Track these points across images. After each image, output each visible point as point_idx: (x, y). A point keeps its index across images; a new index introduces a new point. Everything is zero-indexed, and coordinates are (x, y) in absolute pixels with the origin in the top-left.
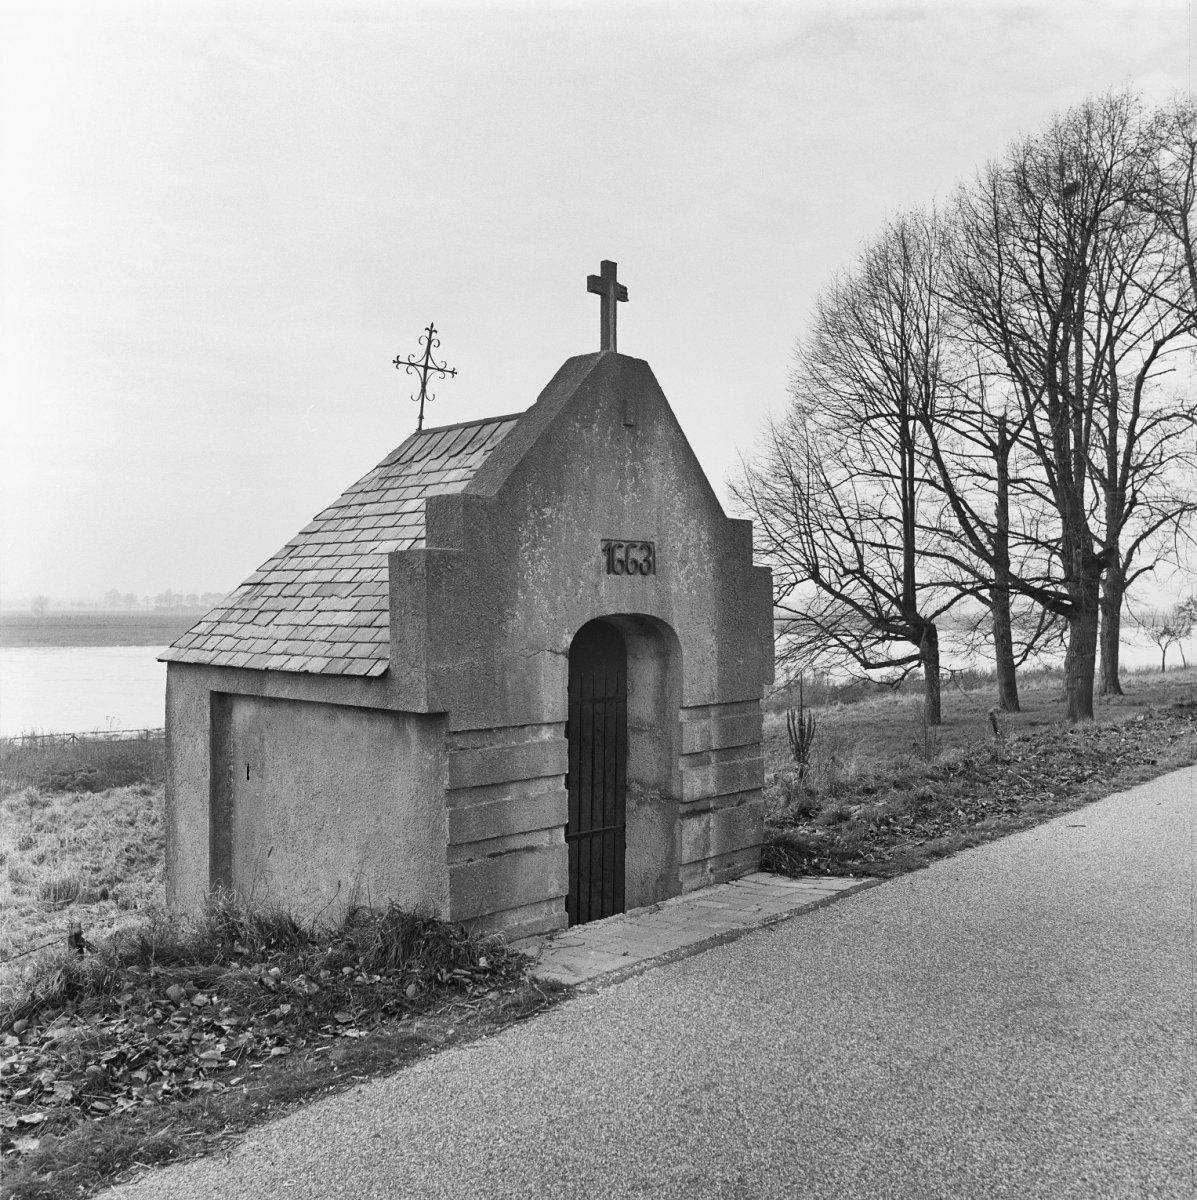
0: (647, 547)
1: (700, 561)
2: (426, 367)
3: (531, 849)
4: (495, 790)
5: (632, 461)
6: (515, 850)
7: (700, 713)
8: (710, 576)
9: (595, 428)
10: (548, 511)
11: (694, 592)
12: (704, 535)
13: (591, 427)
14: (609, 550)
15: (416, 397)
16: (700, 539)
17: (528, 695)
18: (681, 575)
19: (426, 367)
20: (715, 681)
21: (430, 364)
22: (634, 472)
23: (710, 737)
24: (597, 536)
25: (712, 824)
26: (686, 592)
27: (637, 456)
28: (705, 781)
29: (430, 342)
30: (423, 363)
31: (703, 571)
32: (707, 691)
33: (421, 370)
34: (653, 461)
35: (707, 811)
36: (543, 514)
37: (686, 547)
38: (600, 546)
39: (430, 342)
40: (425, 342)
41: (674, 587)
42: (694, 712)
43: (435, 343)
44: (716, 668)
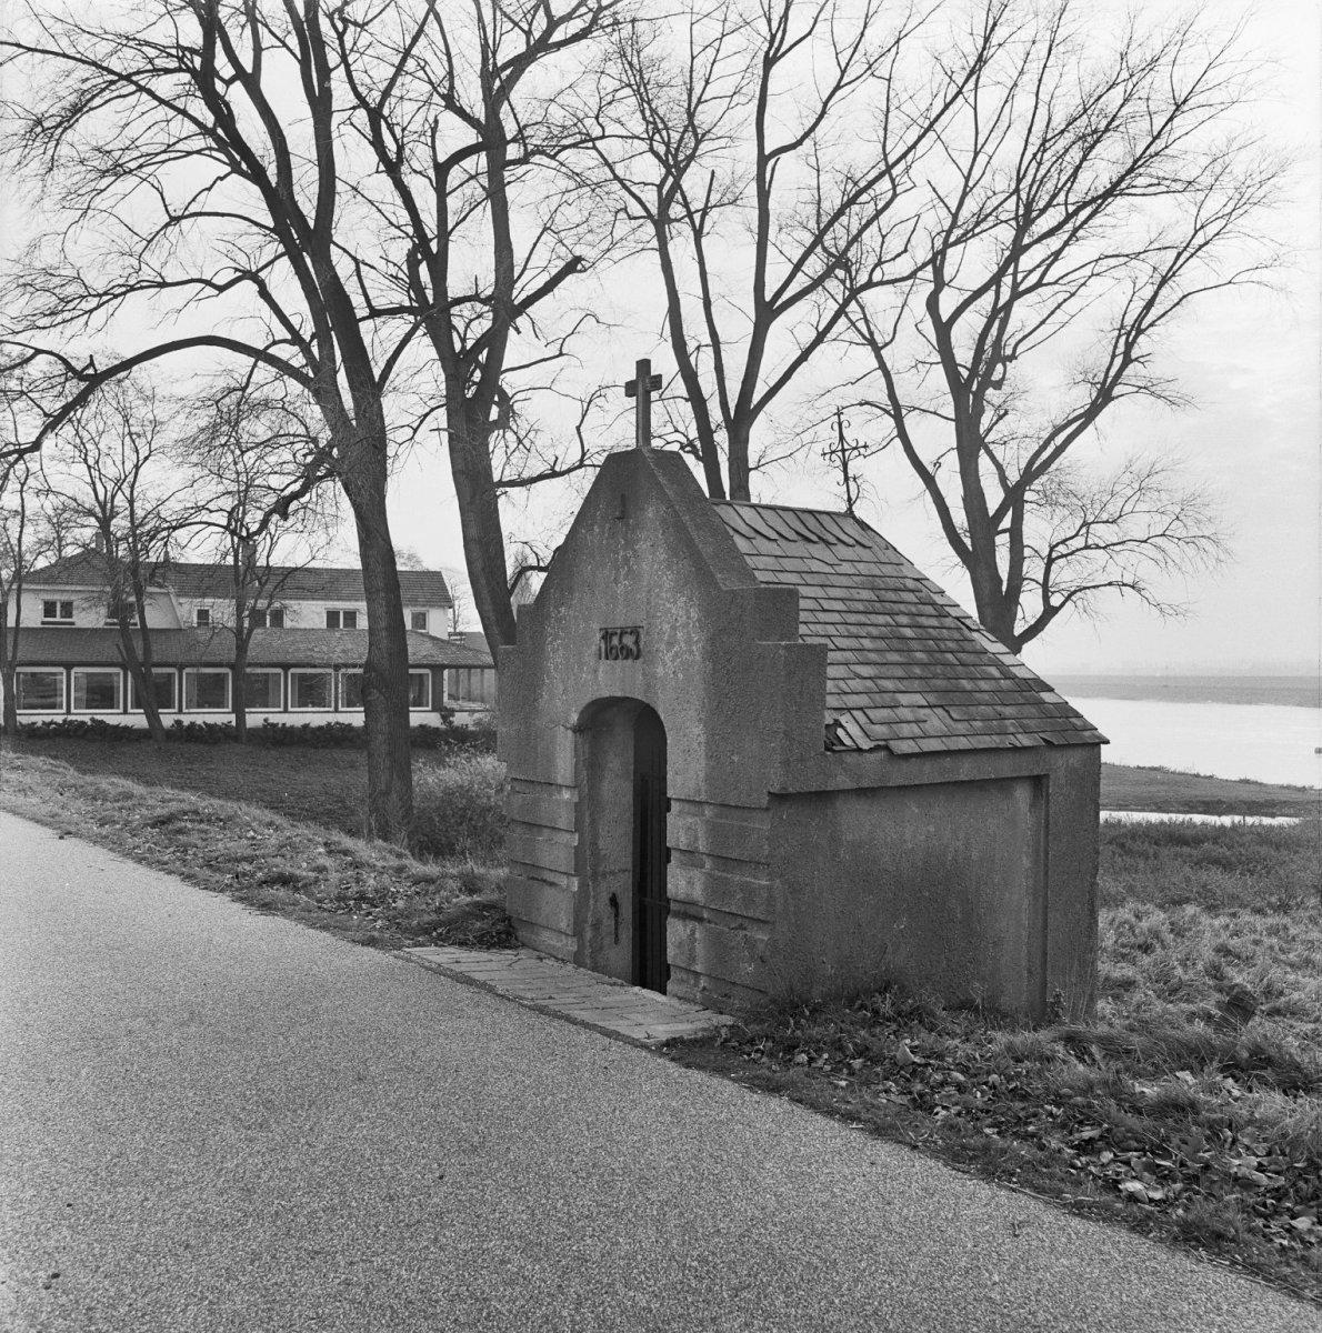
0: (635, 631)
1: (689, 641)
2: (843, 451)
3: (552, 884)
4: (535, 829)
5: (625, 550)
6: (545, 881)
7: (693, 809)
8: (698, 658)
9: (596, 529)
10: (563, 609)
11: (681, 676)
12: (694, 614)
13: (593, 529)
14: (607, 635)
15: (841, 483)
16: (688, 618)
17: (550, 759)
18: (668, 657)
19: (843, 451)
20: (702, 775)
21: (846, 447)
22: (626, 560)
23: (696, 839)
24: (596, 626)
25: (697, 935)
26: (672, 676)
27: (630, 544)
28: (690, 883)
29: (840, 424)
30: (840, 448)
31: (691, 652)
32: (692, 784)
33: (840, 454)
34: (643, 546)
35: (700, 920)
36: (559, 612)
37: (674, 628)
38: (598, 636)
39: (840, 424)
40: (836, 427)
41: (660, 671)
42: (687, 806)
43: (845, 424)
44: (703, 762)
